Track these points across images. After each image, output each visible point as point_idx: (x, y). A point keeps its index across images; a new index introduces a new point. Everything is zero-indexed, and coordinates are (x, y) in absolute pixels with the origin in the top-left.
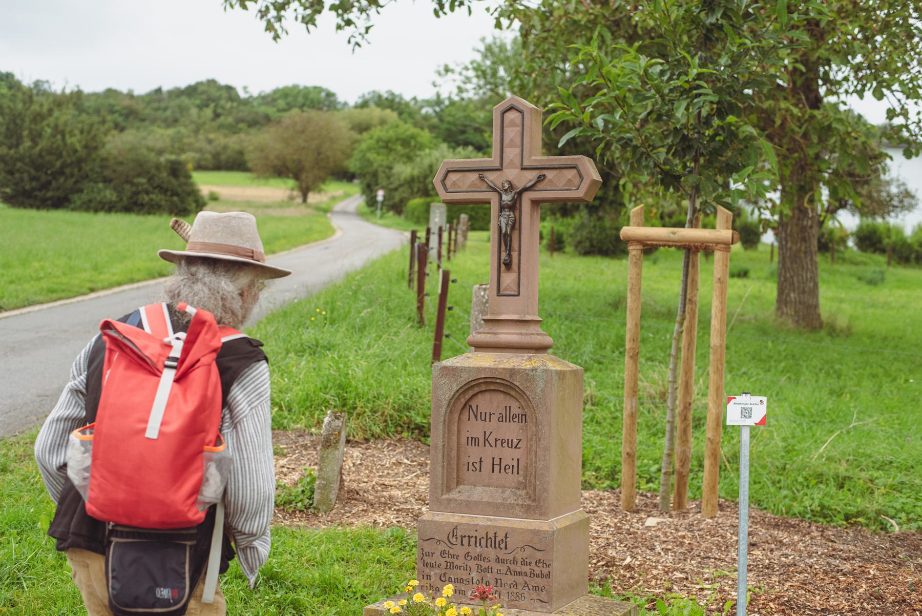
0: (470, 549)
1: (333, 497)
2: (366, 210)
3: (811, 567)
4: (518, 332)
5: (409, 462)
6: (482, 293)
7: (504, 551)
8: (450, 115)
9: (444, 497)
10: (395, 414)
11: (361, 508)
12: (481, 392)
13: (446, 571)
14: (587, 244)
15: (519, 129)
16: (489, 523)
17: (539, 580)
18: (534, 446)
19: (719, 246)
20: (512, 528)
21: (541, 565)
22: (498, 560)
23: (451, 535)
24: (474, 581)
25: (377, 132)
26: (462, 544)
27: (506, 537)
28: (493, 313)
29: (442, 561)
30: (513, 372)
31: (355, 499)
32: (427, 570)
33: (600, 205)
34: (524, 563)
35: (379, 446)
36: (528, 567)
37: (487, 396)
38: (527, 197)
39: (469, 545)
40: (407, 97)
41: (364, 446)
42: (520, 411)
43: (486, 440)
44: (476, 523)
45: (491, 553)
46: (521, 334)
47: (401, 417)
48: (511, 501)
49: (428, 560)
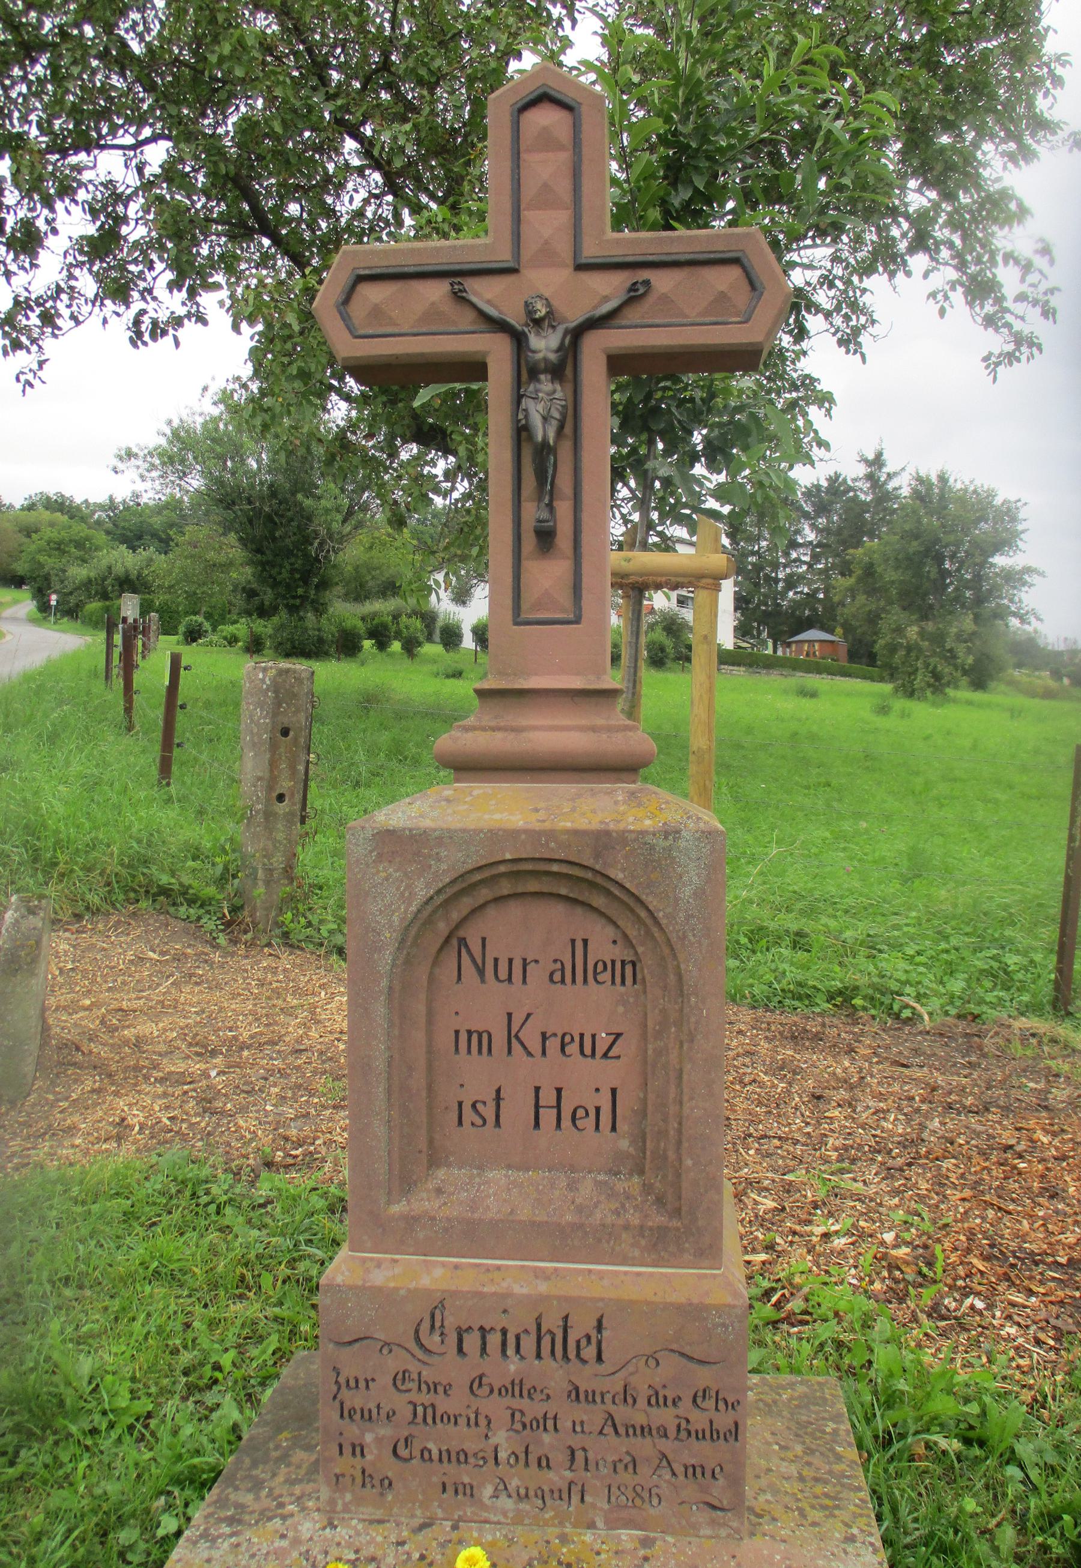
1: (29, 1068)
2: (39, 615)
3: (952, 1143)
4: (583, 722)
5: (155, 956)
7: (592, 1367)
8: (125, 520)
9: (396, 1209)
10: (124, 872)
11: (89, 1085)
12: (497, 900)
13: (414, 1430)
14: (289, 646)
15: (564, 157)
16: (543, 1287)
17: (706, 1445)
18: (674, 1056)
19: (704, 581)
21: (710, 1403)
22: (575, 1394)
23: (426, 1325)
24: (502, 1455)
25: (48, 533)
27: (599, 1327)
28: (501, 674)
29: (399, 1402)
30: (604, 840)
31: (75, 1064)
32: (352, 1430)
33: (302, 604)
34: (656, 1399)
35: (100, 926)
36: (671, 1411)
37: (515, 911)
38: (595, 348)
40: (78, 500)
41: (74, 928)
42: (618, 953)
43: (512, 1037)
45: (554, 1375)
46: (594, 729)
48: (603, 1214)
49: (355, 1399)
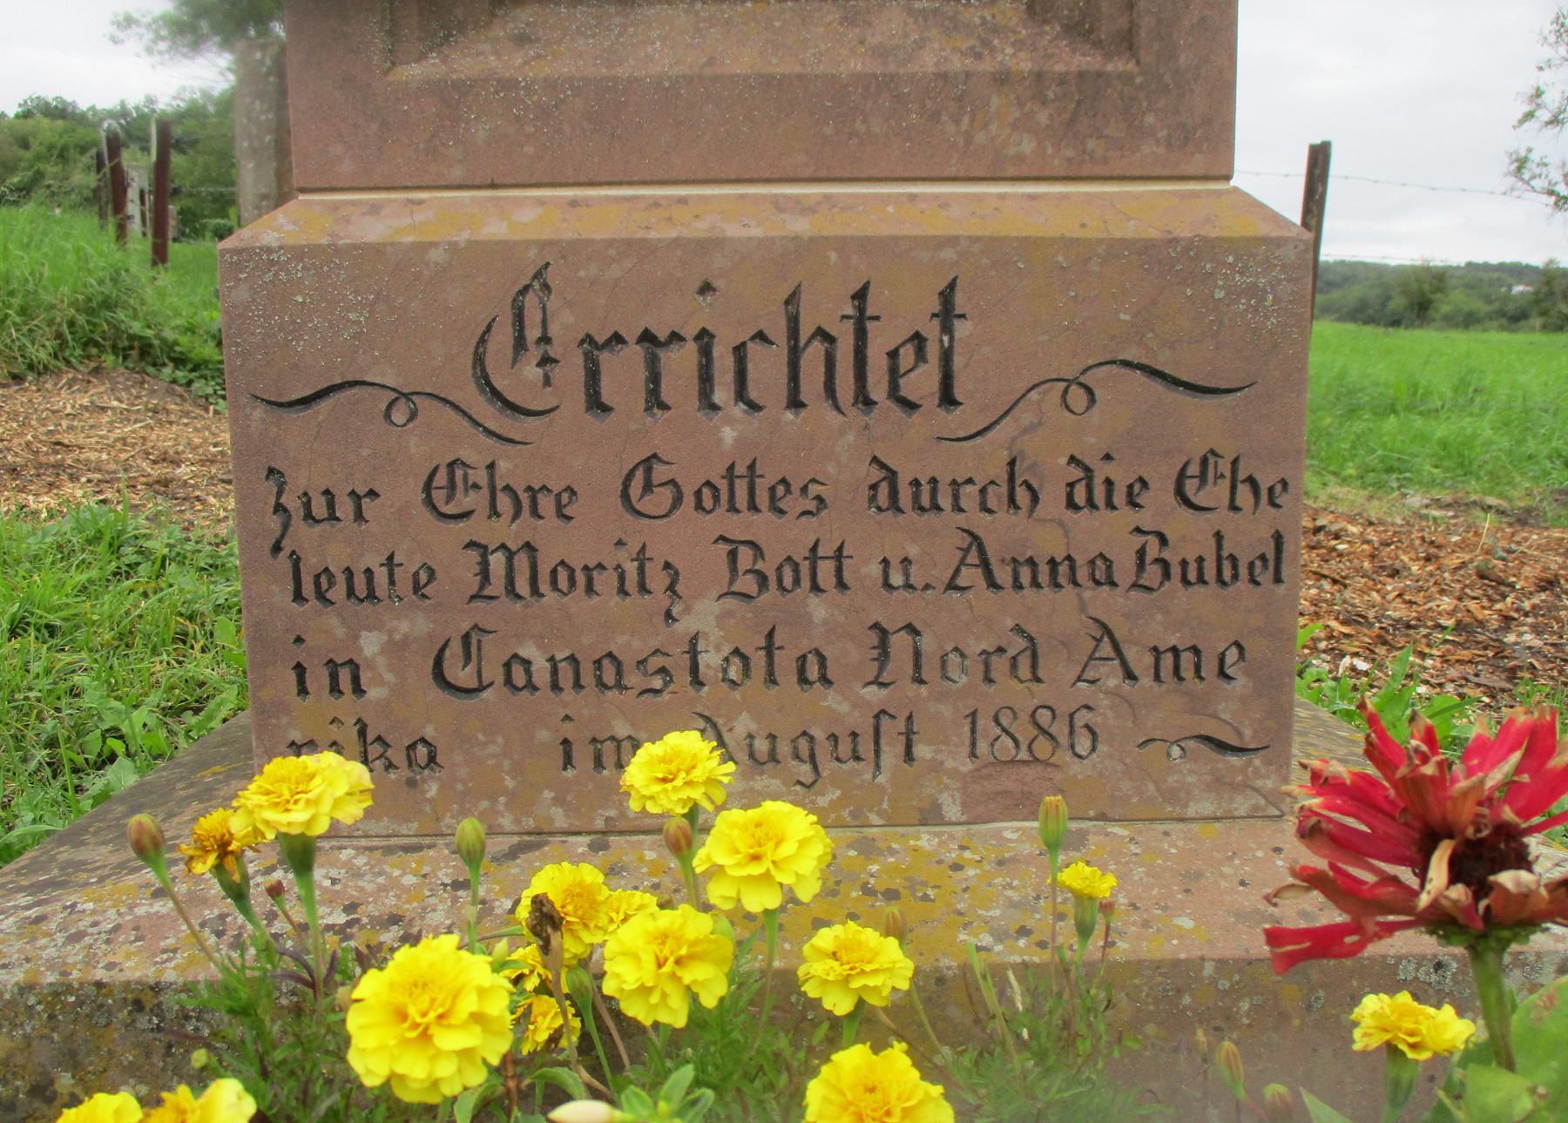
0: (659, 434)
6: (258, 55)
10: (81, 319)
13: (482, 613)
16: (800, 226)
17: (1204, 598)
20: (992, 245)
22: (887, 490)
23: (502, 339)
24: (710, 660)
26: (596, 404)
27: (947, 314)
29: (444, 547)
32: (328, 629)
34: (1088, 490)
36: (1126, 517)
39: (655, 401)
44: (699, 229)
45: (834, 444)
47: (95, 325)
49: (325, 548)
